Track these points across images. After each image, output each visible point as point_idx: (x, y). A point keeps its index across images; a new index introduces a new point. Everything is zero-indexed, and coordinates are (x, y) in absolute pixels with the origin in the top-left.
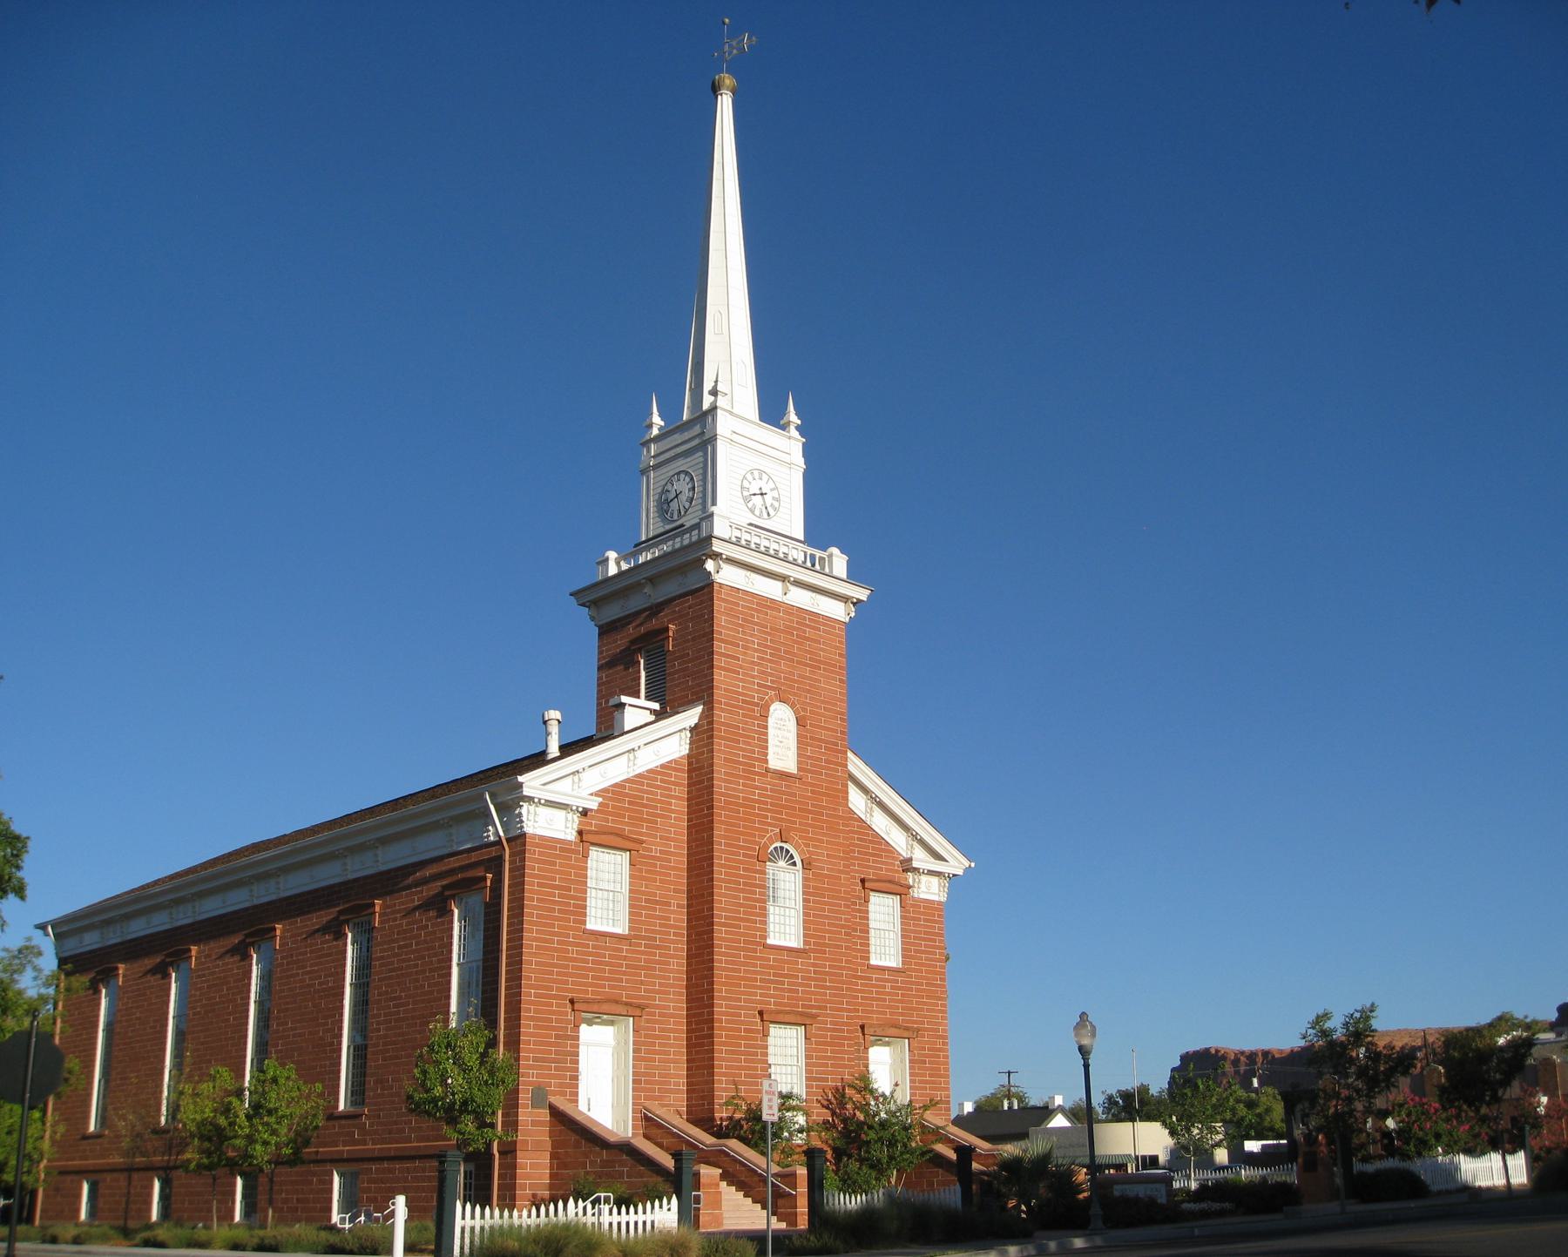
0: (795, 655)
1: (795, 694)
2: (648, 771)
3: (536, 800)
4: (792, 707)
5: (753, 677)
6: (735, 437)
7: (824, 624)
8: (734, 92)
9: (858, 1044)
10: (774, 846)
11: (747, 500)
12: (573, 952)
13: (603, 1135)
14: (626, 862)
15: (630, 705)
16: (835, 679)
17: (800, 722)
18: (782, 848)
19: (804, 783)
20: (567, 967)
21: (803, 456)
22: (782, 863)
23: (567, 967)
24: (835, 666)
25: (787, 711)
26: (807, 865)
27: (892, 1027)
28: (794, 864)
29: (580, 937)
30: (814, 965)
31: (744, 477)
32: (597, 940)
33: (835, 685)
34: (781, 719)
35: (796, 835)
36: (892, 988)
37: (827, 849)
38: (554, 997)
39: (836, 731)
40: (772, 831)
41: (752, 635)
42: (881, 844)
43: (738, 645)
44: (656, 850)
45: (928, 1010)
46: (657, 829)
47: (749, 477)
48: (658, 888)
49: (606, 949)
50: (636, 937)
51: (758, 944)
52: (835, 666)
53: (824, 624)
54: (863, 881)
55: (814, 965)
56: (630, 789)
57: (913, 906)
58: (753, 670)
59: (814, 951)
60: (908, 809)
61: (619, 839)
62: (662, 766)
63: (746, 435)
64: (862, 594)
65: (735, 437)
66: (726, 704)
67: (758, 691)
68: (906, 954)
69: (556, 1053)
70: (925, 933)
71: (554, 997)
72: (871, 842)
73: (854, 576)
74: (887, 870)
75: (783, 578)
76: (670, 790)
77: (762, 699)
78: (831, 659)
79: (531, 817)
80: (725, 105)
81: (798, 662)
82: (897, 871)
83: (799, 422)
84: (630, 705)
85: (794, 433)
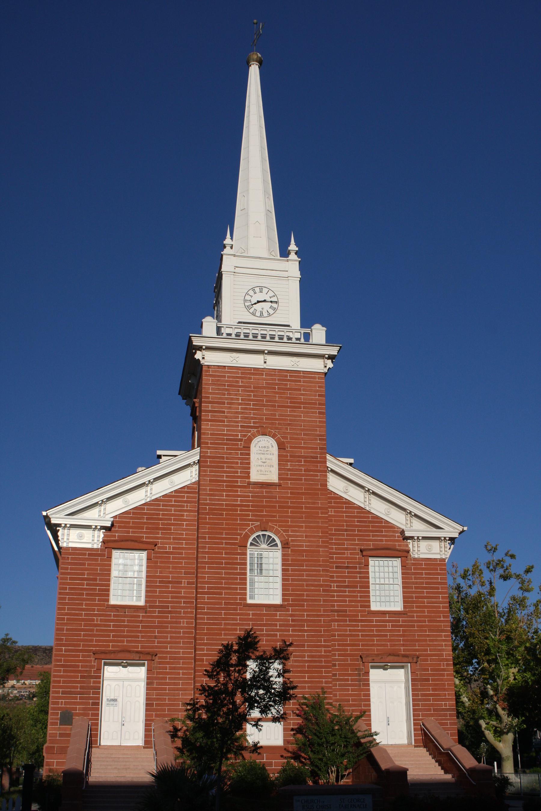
0: (275, 401)
1: (277, 428)
2: (163, 496)
3: (416, 538)
4: (273, 437)
5: (237, 422)
6: (237, 270)
7: (304, 377)
8: (260, 63)
9: (360, 670)
10: (273, 536)
11: (248, 308)
12: (97, 620)
13: (454, 751)
14: (399, 565)
15: (164, 456)
16: (316, 413)
17: (281, 447)
18: (264, 535)
19: (284, 488)
20: (92, 630)
21: (299, 270)
22: (264, 546)
23: (92, 630)
24: (315, 404)
25: (268, 439)
26: (285, 545)
27: (390, 655)
28: (276, 545)
29: (103, 610)
30: (291, 615)
31: (247, 294)
32: (118, 611)
33: (316, 417)
34: (265, 447)
35: (276, 525)
36: (392, 626)
37: (305, 531)
38: (81, 651)
39: (316, 448)
40: (252, 524)
41: (236, 395)
42: (381, 522)
43: (224, 403)
44: (169, 548)
45: (430, 641)
46: (171, 534)
47: (251, 292)
48: (171, 573)
49: (125, 616)
50: (150, 607)
51: (240, 604)
52: (315, 404)
53: (304, 377)
54: (361, 551)
55: (291, 615)
56: (148, 509)
57: (414, 564)
58: (238, 417)
59: (291, 605)
60: (398, 496)
61: (136, 544)
62: (176, 491)
63: (248, 267)
64: (333, 351)
65: (237, 270)
66: (211, 443)
67: (241, 431)
68: (406, 600)
69: (81, 688)
70: (427, 583)
71: (81, 651)
72: (370, 522)
73: (330, 340)
74: (386, 541)
75: (261, 352)
76: (183, 506)
77: (245, 436)
78: (312, 399)
79: (416, 549)
80: (254, 71)
81: (279, 406)
82: (398, 541)
83: (297, 249)
84: (164, 456)
85: (293, 256)
